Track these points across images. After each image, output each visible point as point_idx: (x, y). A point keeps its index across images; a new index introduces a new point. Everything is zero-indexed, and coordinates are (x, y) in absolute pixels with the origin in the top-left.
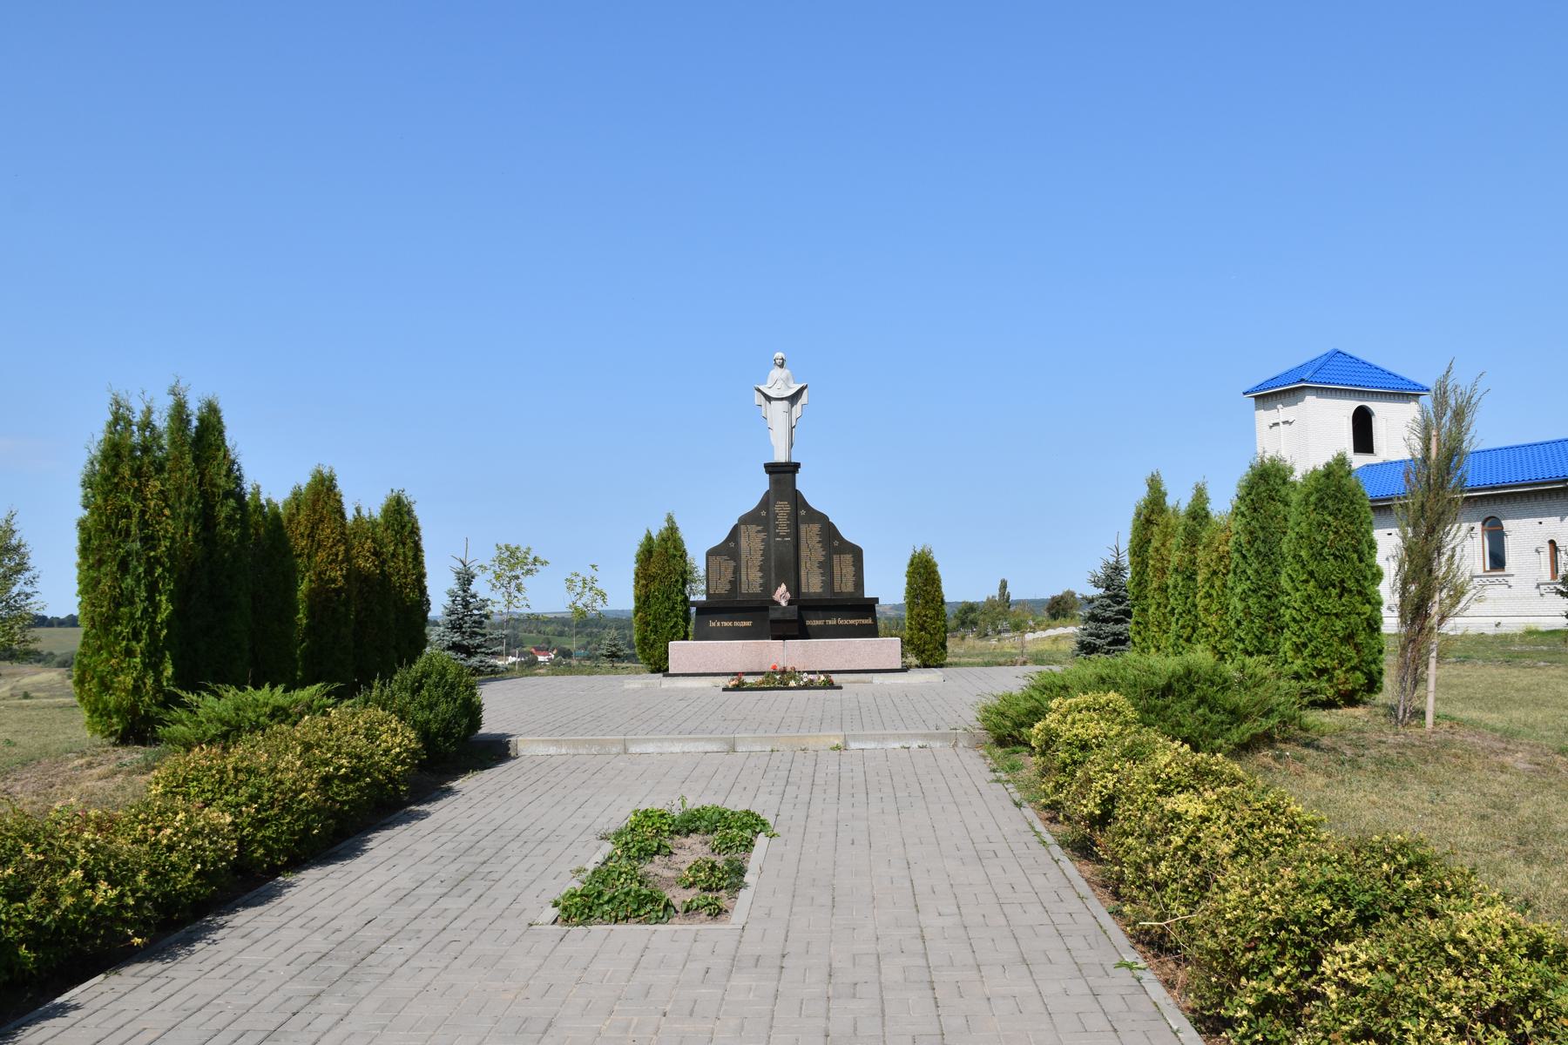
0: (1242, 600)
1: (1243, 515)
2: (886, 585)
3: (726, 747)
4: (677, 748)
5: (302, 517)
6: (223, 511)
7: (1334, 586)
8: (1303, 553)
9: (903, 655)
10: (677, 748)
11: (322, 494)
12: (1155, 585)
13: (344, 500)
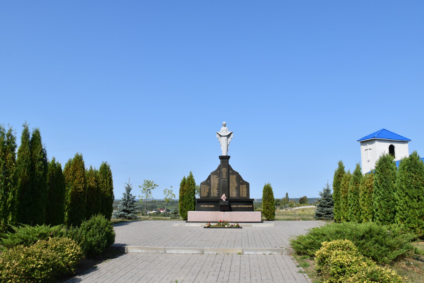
0: (378, 202)
1: (378, 173)
2: (256, 194)
3: (200, 252)
4: (183, 252)
5: (71, 169)
6: (38, 165)
7: (415, 198)
8: (403, 186)
9: (262, 217)
10: (183, 252)
11: (78, 162)
12: (342, 196)
13: (85, 164)
